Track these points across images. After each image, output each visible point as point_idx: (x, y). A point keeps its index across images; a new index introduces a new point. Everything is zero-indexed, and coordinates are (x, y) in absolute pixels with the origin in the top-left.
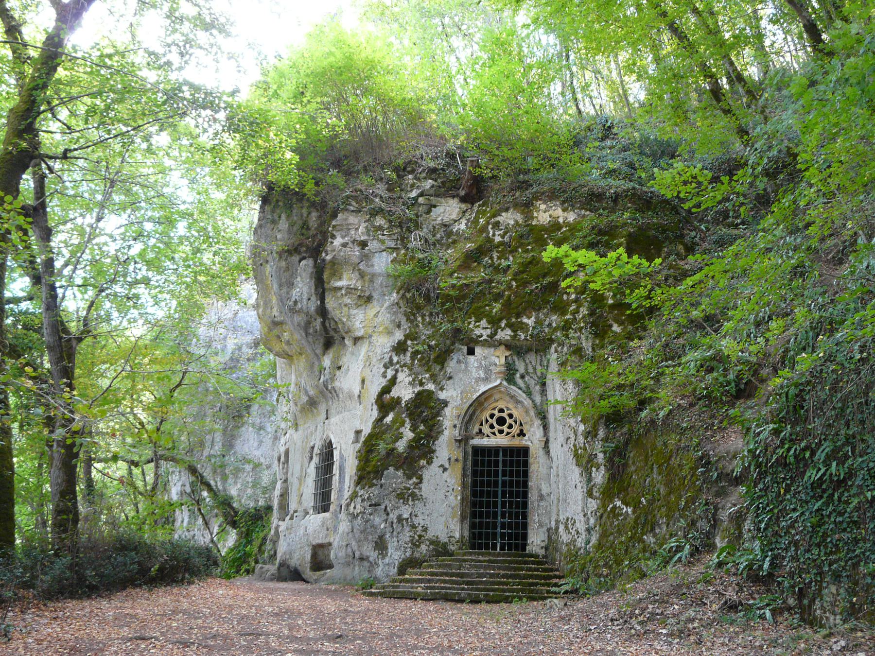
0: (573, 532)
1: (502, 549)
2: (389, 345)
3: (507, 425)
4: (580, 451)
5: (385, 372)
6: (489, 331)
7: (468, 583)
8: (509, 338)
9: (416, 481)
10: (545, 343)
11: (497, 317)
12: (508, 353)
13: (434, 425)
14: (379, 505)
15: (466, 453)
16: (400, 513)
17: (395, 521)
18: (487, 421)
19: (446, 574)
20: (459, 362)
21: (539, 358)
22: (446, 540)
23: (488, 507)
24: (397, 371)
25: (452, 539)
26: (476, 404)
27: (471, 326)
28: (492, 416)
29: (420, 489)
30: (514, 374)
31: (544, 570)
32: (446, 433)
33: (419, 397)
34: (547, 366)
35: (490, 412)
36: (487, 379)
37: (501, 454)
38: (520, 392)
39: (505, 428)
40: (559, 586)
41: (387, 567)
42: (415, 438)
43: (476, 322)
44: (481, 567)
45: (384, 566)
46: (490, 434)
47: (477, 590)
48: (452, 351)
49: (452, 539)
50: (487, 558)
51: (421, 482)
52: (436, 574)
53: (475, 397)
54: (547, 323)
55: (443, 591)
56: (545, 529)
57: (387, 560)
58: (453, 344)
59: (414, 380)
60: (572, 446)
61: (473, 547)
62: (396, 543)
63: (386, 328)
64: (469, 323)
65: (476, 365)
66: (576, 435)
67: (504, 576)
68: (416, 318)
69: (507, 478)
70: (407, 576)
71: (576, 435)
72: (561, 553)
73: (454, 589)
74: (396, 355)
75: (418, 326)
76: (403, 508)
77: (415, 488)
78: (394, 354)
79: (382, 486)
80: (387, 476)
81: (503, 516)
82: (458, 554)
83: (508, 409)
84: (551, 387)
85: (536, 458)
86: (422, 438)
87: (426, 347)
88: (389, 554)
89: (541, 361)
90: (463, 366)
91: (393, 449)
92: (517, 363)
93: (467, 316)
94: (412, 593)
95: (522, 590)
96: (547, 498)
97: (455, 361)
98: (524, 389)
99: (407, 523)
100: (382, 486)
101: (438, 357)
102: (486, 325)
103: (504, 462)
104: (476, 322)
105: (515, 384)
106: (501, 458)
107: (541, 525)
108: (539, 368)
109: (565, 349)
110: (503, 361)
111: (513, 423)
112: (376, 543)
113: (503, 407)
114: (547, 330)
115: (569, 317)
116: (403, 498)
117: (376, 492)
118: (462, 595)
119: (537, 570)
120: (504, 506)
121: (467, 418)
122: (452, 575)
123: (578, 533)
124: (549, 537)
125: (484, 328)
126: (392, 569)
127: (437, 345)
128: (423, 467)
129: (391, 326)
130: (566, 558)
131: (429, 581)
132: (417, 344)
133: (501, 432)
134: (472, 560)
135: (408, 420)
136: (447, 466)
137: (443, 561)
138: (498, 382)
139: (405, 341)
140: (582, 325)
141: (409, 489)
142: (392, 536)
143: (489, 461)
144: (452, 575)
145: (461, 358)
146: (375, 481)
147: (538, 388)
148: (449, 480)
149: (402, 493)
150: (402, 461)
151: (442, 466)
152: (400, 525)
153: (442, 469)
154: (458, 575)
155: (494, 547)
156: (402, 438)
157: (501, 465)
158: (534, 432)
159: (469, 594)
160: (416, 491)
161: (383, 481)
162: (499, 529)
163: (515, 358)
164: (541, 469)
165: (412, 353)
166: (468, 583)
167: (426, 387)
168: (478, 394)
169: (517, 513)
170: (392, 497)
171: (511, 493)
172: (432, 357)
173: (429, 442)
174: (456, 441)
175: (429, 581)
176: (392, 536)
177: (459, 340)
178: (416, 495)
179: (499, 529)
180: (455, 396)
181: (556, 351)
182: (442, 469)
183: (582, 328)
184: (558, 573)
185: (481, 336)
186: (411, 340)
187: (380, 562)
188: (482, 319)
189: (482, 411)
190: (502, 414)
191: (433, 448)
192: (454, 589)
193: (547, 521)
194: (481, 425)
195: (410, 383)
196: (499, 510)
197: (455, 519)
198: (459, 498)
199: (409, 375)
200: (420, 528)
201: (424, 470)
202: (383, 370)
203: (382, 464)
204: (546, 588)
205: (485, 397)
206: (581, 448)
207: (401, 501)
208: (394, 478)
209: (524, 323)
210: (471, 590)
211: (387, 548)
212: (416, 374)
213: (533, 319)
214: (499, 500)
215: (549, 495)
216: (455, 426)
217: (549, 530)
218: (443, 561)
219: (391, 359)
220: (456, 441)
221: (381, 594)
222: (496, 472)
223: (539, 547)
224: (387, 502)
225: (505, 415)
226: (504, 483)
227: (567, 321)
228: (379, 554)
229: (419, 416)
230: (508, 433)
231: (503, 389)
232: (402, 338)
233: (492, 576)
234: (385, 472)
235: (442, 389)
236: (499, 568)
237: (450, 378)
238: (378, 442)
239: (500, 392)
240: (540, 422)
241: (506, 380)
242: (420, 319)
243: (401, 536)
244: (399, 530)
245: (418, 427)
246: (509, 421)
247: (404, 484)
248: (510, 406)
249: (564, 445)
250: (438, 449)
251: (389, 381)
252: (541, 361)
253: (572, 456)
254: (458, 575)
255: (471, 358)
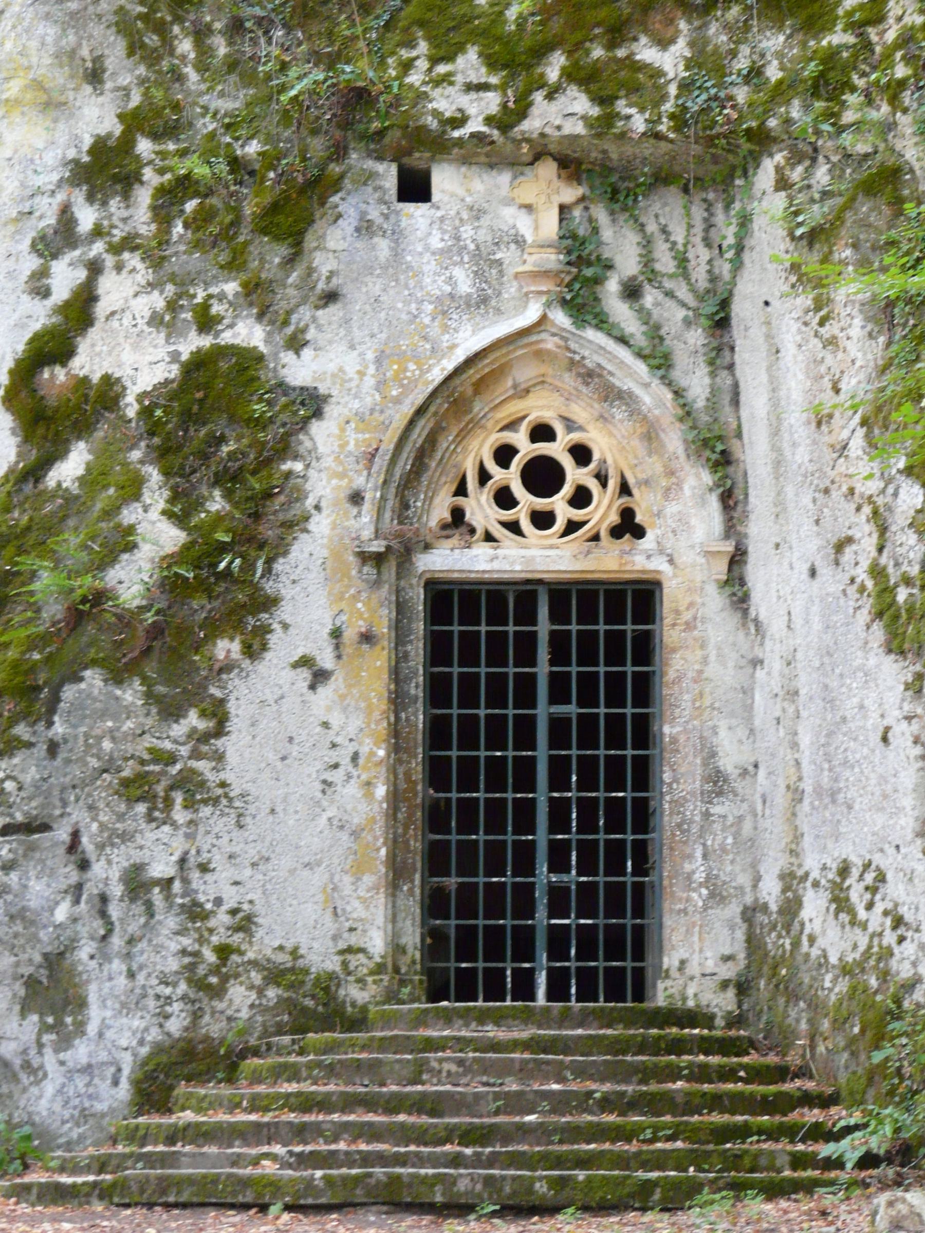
0: (876, 920)
1: (557, 992)
2: (52, 157)
3: (567, 490)
4: (902, 595)
5: (42, 273)
6: (492, 102)
7: (468, 1136)
8: (579, 129)
9: (202, 725)
10: (732, 149)
11: (527, 42)
12: (570, 194)
13: (268, 495)
14: (45, 827)
15: (401, 607)
16: (137, 857)
17: (117, 890)
18: (484, 477)
19: (367, 1103)
20: (366, 228)
21: (698, 213)
22: (333, 964)
23: (495, 824)
24: (95, 268)
25: (355, 961)
26: (441, 405)
27: (415, 78)
28: (504, 455)
29: (219, 757)
30: (598, 281)
31: (316, 1131)
32: (320, 525)
33: (201, 376)
34: (740, 248)
35: (495, 438)
36: (484, 300)
37: (543, 612)
38: (623, 353)
39: (559, 504)
40: (837, 1137)
41: (80, 1082)
42: (187, 548)
43: (435, 61)
44: (505, 1069)
45: (70, 1074)
46: (499, 532)
47: (515, 1160)
48: (336, 185)
49: (355, 961)
50: (524, 1034)
51: (220, 731)
52: (323, 1104)
53: (437, 375)
54: (742, 63)
55: (379, 1171)
56: (734, 910)
57: (81, 1052)
58: (339, 152)
59: (172, 306)
60: (862, 575)
61: (436, 993)
62: (122, 981)
63: (38, 85)
64: (407, 66)
65: (436, 242)
66: (883, 530)
67: (607, 1104)
68: (168, 44)
69: (572, 709)
70: (188, 1116)
71: (883, 530)
72: (815, 1006)
73: (421, 1160)
74: (90, 198)
75: (180, 78)
76: (149, 835)
77: (196, 755)
78: (78, 196)
79: (53, 748)
80: (78, 706)
81: (558, 863)
82: (388, 1020)
83: (570, 425)
84: (757, 333)
85: (689, 626)
86: (223, 548)
87: (223, 168)
88: (92, 1028)
89: (709, 226)
90: (383, 246)
91: (99, 597)
92: (607, 234)
93: (395, 37)
94: (245, 1183)
95: (698, 1159)
96: (739, 785)
97: (347, 225)
98: (640, 340)
99: (169, 897)
100: (53, 748)
101: (275, 208)
102: (480, 74)
103: (558, 642)
104: (435, 61)
105: (602, 322)
106: (544, 627)
107: (717, 896)
108: (700, 255)
109: (822, 176)
110: (550, 225)
111: (593, 485)
112: (31, 983)
113: (549, 416)
114: (742, 95)
115: (839, 37)
116: (148, 797)
117: (31, 775)
118: (463, 1185)
119: (728, 1074)
120: (558, 820)
121: (405, 463)
122: (393, 1105)
123: (898, 922)
124: (753, 943)
125: (470, 88)
126: (103, 1086)
127: (270, 160)
128: (227, 667)
129: (59, 78)
130: (839, 1024)
131: (301, 1132)
132: (183, 153)
133: (543, 520)
134: (462, 1043)
135: (154, 474)
136: (326, 660)
137: (330, 1048)
138: (532, 314)
139: (127, 143)
140: (901, 71)
141: (172, 759)
142: (102, 955)
143: (497, 642)
144: (393, 1105)
145: (374, 214)
146: (21, 730)
147: (697, 337)
148: (336, 720)
149: (141, 778)
150: (140, 642)
151: (305, 662)
152: (138, 908)
153: (305, 674)
154: (420, 1105)
155: (525, 990)
156: (131, 547)
157: (543, 654)
158: (682, 519)
159: (489, 1181)
160: (202, 765)
161: (59, 728)
162: (541, 913)
163: (601, 214)
164: (713, 670)
165: (161, 191)
166: (468, 1136)
167: (227, 338)
168: (450, 365)
169: (616, 852)
170: (100, 795)
171: (588, 767)
172: (248, 210)
173: (248, 567)
174: (364, 557)
175: (301, 1132)
176: (102, 955)
177: (364, 137)
178: (202, 784)
179: (541, 913)
180: (351, 370)
181: (782, 184)
182: (305, 674)
183: (902, 84)
184: (810, 1085)
185: (459, 121)
186: (155, 137)
187: (49, 1059)
188: (460, 48)
189: (463, 436)
190: (544, 448)
191: (269, 587)
192: (421, 1160)
193: (744, 880)
194: (461, 490)
195: (156, 320)
196: (541, 837)
197: (368, 880)
198: (381, 791)
199: (151, 286)
200: (222, 919)
201: (234, 681)
202: (32, 263)
203: (48, 660)
204: (783, 1145)
205: (473, 374)
206: (907, 581)
207: (141, 808)
208: (103, 715)
209: (643, 67)
210: (492, 1161)
211: (82, 1004)
212: (183, 282)
213: (681, 48)
214: (542, 796)
215: (748, 772)
216: (356, 498)
217: (749, 914)
218: (330, 1048)
219: (66, 219)
220: (364, 557)
221: (104, 1193)
222: (527, 685)
223: (710, 983)
224: (78, 815)
225: (557, 450)
226: (558, 727)
227: (830, 57)
228: (45, 1028)
229: (204, 457)
230: (572, 527)
231: (550, 343)
232: (111, 126)
233: (560, 1103)
234: (69, 693)
235: (296, 344)
236: (581, 1072)
237: (331, 297)
238: (27, 562)
239: (540, 355)
240: (707, 478)
241: (564, 303)
242: (185, 46)
243: (144, 953)
244: (133, 928)
245: (199, 504)
246: (574, 475)
247: (149, 741)
248: (580, 412)
249: (825, 571)
250: (287, 592)
251: (64, 309)
252: (709, 226)
253: (864, 616)
254: (420, 1105)
255: (416, 212)
